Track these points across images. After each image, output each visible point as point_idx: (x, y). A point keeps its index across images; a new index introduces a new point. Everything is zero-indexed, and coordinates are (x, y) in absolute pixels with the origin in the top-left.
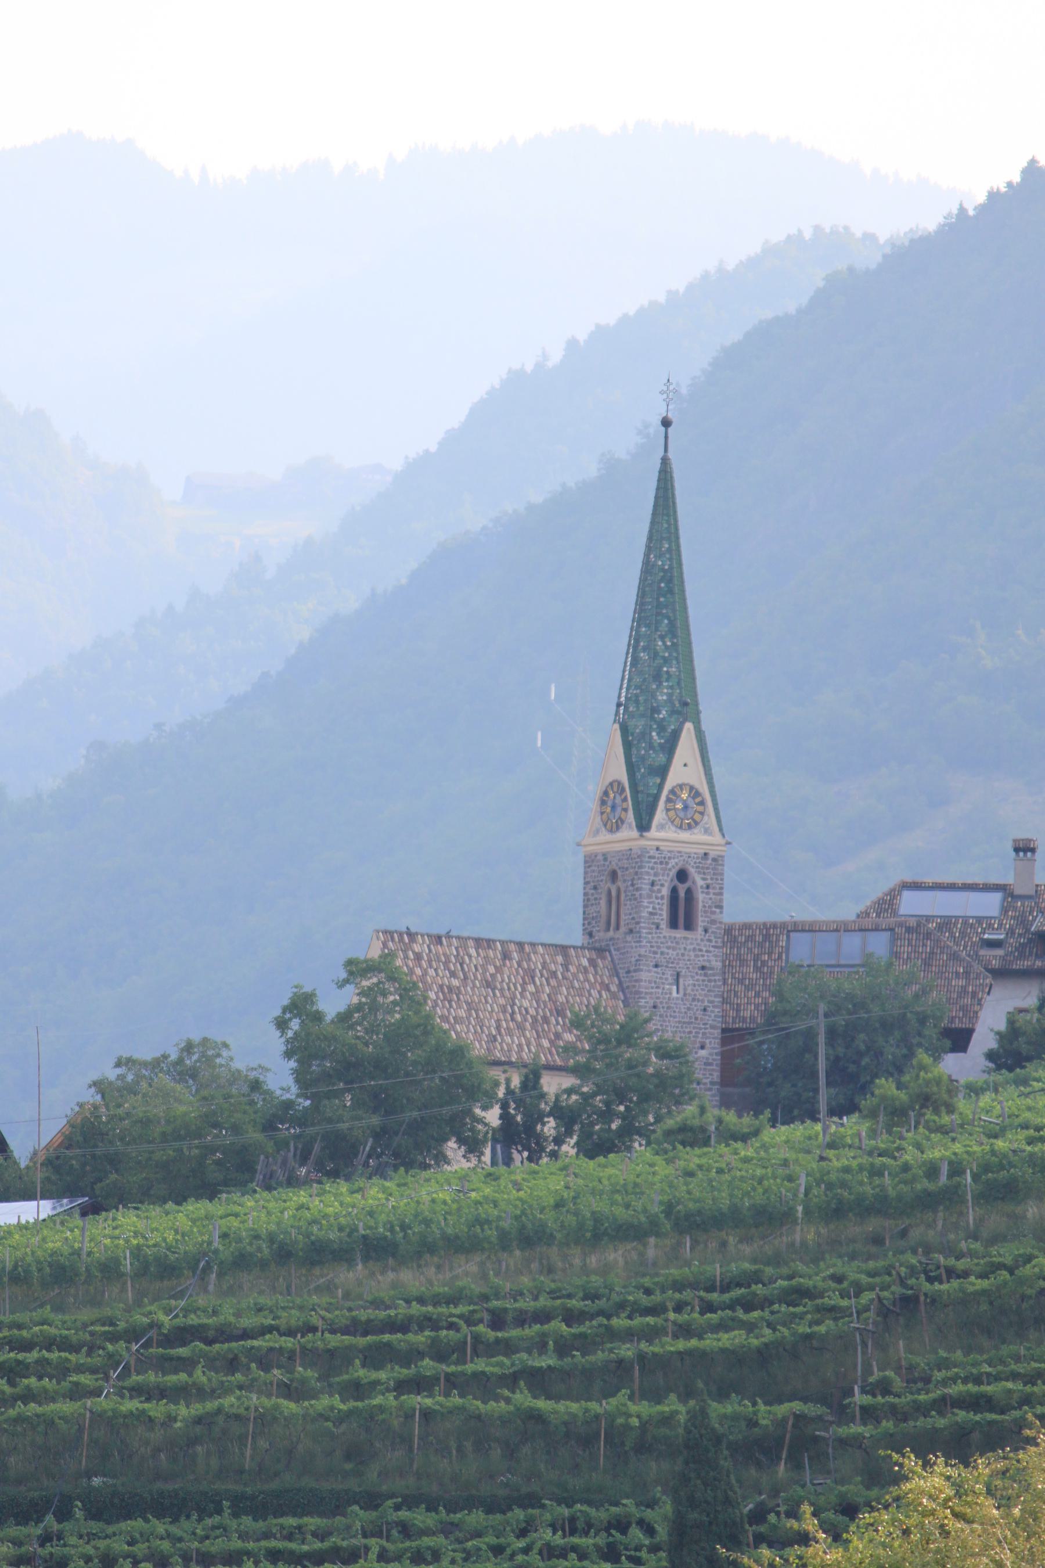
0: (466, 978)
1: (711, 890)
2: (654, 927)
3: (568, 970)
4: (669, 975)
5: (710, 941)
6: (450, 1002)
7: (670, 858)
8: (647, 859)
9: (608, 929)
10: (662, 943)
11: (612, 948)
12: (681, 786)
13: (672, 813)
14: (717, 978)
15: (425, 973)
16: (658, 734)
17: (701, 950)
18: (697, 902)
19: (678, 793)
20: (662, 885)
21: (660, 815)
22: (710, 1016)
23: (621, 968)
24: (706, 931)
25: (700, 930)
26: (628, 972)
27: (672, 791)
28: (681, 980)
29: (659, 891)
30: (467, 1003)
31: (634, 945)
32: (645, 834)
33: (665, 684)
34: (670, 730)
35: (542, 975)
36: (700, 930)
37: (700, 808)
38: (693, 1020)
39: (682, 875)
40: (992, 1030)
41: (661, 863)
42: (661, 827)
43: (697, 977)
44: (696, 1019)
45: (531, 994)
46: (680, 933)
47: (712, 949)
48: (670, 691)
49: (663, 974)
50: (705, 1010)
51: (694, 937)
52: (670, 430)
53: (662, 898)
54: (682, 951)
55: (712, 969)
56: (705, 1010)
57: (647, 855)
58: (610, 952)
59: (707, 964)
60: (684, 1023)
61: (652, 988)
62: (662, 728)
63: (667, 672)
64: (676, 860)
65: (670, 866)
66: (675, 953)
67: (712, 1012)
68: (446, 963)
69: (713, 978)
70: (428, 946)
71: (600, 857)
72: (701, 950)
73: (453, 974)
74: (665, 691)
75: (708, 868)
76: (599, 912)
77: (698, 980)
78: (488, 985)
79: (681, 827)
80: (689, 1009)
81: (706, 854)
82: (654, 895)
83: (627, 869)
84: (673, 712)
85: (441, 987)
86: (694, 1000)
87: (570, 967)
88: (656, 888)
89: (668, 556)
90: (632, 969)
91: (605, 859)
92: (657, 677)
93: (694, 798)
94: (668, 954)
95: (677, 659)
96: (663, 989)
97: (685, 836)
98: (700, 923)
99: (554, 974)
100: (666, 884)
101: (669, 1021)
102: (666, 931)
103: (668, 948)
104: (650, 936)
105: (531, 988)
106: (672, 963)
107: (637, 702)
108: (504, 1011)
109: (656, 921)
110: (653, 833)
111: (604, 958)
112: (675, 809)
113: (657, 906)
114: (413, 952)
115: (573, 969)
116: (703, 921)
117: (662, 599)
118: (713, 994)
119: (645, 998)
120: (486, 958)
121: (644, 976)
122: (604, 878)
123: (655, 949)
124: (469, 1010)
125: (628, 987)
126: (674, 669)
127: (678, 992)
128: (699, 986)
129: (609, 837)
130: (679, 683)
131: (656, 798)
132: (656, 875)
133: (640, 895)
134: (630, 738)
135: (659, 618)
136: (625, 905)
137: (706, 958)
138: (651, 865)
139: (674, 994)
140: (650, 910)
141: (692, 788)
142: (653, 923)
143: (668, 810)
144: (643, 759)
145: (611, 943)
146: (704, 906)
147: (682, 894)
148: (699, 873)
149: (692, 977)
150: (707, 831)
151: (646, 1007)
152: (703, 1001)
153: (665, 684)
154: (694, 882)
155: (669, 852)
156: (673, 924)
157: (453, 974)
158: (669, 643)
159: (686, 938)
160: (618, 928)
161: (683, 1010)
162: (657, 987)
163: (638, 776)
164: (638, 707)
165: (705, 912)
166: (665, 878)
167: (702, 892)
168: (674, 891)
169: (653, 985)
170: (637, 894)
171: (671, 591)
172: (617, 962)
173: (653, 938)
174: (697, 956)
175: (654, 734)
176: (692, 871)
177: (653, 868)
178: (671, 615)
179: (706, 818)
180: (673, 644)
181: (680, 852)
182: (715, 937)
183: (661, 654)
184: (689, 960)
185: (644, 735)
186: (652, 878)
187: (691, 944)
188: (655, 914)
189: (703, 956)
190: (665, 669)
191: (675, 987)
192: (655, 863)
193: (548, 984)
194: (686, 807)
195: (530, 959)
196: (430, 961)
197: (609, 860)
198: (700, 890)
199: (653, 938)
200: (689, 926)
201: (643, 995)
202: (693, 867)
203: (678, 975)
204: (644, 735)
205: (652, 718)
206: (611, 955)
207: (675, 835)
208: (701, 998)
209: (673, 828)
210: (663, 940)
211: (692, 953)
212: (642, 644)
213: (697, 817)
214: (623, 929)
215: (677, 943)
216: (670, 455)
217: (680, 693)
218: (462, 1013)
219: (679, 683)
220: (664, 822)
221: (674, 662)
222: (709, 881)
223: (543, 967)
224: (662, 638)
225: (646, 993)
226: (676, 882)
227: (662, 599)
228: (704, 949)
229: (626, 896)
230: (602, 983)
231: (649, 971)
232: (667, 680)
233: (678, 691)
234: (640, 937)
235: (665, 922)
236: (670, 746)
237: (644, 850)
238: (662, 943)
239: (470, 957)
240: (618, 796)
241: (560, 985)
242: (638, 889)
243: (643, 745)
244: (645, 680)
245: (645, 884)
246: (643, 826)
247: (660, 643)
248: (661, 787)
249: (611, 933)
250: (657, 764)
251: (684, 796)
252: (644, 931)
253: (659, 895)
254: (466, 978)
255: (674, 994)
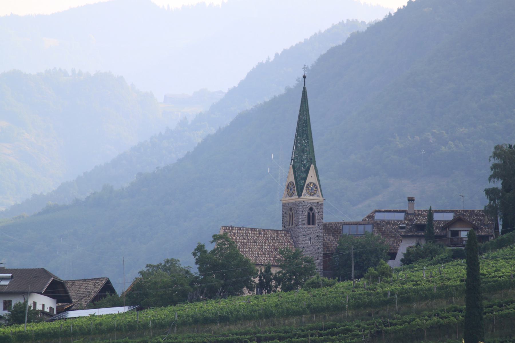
0: (248, 240)
1: (319, 213)
2: (303, 224)
3: (278, 237)
4: (308, 238)
5: (319, 228)
6: (244, 247)
7: (307, 204)
8: (301, 204)
9: (290, 225)
10: (306, 229)
11: (291, 231)
12: (310, 183)
13: (308, 191)
14: (322, 239)
15: (236, 238)
16: (303, 168)
17: (317, 231)
18: (316, 217)
19: (310, 185)
20: (305, 212)
21: (304, 192)
22: (320, 250)
23: (294, 236)
24: (318, 225)
25: (317, 225)
26: (296, 237)
27: (308, 185)
28: (311, 240)
29: (304, 214)
30: (249, 247)
31: (297, 229)
32: (300, 197)
33: (305, 153)
34: (307, 167)
35: (271, 239)
36: (317, 225)
37: (316, 189)
38: (315, 251)
39: (311, 209)
40: (402, 253)
41: (305, 205)
42: (305, 195)
43: (316, 239)
44: (316, 251)
45: (267, 244)
46: (311, 226)
47: (320, 230)
48: (307, 155)
49: (306, 238)
50: (318, 248)
51: (315, 227)
52: (305, 79)
53: (305, 216)
54: (311, 231)
55: (320, 236)
56: (318, 248)
57: (301, 203)
58: (290, 232)
59: (319, 235)
60: (312, 252)
61: (303, 242)
62: (304, 166)
63: (306, 150)
64: (309, 205)
65: (307, 206)
66: (309, 232)
67: (320, 249)
68: (242, 236)
69: (320, 239)
70: (237, 231)
71: (287, 204)
72: (317, 231)
73: (245, 239)
74: (305, 155)
75: (319, 207)
76: (287, 220)
77: (316, 240)
78: (255, 242)
79: (310, 195)
80: (313, 248)
81: (318, 203)
82: (303, 215)
83: (295, 207)
84: (308, 161)
85: (241, 243)
86: (315, 245)
87: (279, 236)
88: (303, 213)
89: (305, 116)
90: (297, 236)
91: (289, 205)
92: (303, 151)
93: (314, 186)
94: (307, 232)
95: (309, 146)
96: (306, 242)
97: (312, 197)
98: (317, 223)
99: (274, 238)
100: (306, 212)
101: (308, 252)
102: (307, 225)
103: (307, 230)
104: (302, 227)
105: (267, 242)
106: (309, 235)
107: (297, 159)
108: (260, 249)
109: (304, 222)
110: (302, 197)
111: (289, 234)
112: (309, 190)
113: (304, 218)
114: (233, 232)
115: (279, 237)
116: (317, 222)
117: (304, 129)
118: (320, 243)
119: (301, 245)
120: (254, 234)
121: (300, 238)
122: (288, 210)
123: (303, 231)
124: (249, 249)
125: (296, 242)
126: (308, 149)
127: (310, 243)
128: (316, 241)
129: (290, 198)
130: (309, 153)
131: (303, 186)
132: (303, 209)
133: (299, 215)
134: (295, 169)
135: (303, 134)
136: (295, 218)
137: (318, 233)
138: (302, 206)
139: (309, 244)
140: (302, 219)
141: (313, 183)
142: (303, 223)
143: (307, 190)
144: (299, 175)
145: (290, 229)
146: (318, 218)
147: (311, 214)
148: (316, 208)
149: (314, 239)
150: (318, 196)
151: (301, 248)
152: (318, 246)
153: (305, 153)
154: (315, 211)
155: (307, 202)
156: (309, 223)
157: (245, 239)
158: (306, 141)
159: (312, 227)
160: (292, 225)
161: (312, 248)
162: (304, 242)
163: (298, 180)
164: (297, 160)
165: (318, 220)
166: (306, 210)
167: (317, 214)
168: (309, 214)
169: (303, 241)
170: (298, 215)
171: (307, 126)
172: (292, 235)
173: (303, 227)
174: (315, 233)
175: (302, 168)
176: (314, 208)
177: (302, 207)
178: (307, 133)
179: (318, 192)
180: (307, 142)
181: (310, 202)
182: (321, 227)
183: (304, 145)
184: (313, 234)
185: (299, 168)
186: (302, 210)
187: (314, 229)
188: (303, 220)
189: (317, 232)
190: (305, 149)
191: (309, 242)
192: (303, 205)
193: (272, 241)
194: (312, 189)
195: (267, 234)
196: (238, 235)
197: (290, 205)
198: (316, 213)
199: (303, 227)
200: (313, 224)
201: (300, 244)
202: (314, 207)
203: (310, 238)
204: (299, 168)
205: (302, 163)
206: (291, 233)
207: (309, 197)
208: (317, 245)
209: (308, 195)
210: (306, 228)
211: (314, 232)
212: (298, 142)
213: (315, 192)
214: (294, 225)
215: (310, 229)
216: (306, 86)
217: (310, 156)
218: (247, 250)
219: (309, 153)
220: (305, 194)
221: (308, 147)
222: (319, 211)
223: (271, 236)
224: (304, 140)
225: (301, 244)
226: (309, 211)
227: (304, 129)
228: (318, 230)
229: (295, 215)
230: (288, 241)
231: (302, 237)
232: (306, 152)
233: (309, 155)
234: (299, 227)
235: (306, 222)
236: (307, 171)
237: (300, 202)
238: (306, 229)
239: (249, 234)
240: (292, 186)
241: (276, 242)
242: (298, 213)
243: (299, 171)
244: (299, 152)
245: (300, 212)
246: (300, 195)
247: (304, 141)
248: (304, 183)
249: (290, 226)
250: (303, 177)
251: (311, 186)
252: (300, 225)
253: (304, 215)
254: (248, 240)
255: (309, 244)
